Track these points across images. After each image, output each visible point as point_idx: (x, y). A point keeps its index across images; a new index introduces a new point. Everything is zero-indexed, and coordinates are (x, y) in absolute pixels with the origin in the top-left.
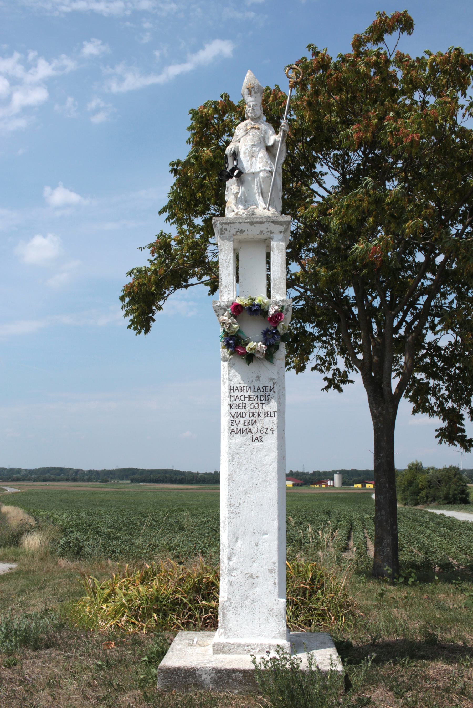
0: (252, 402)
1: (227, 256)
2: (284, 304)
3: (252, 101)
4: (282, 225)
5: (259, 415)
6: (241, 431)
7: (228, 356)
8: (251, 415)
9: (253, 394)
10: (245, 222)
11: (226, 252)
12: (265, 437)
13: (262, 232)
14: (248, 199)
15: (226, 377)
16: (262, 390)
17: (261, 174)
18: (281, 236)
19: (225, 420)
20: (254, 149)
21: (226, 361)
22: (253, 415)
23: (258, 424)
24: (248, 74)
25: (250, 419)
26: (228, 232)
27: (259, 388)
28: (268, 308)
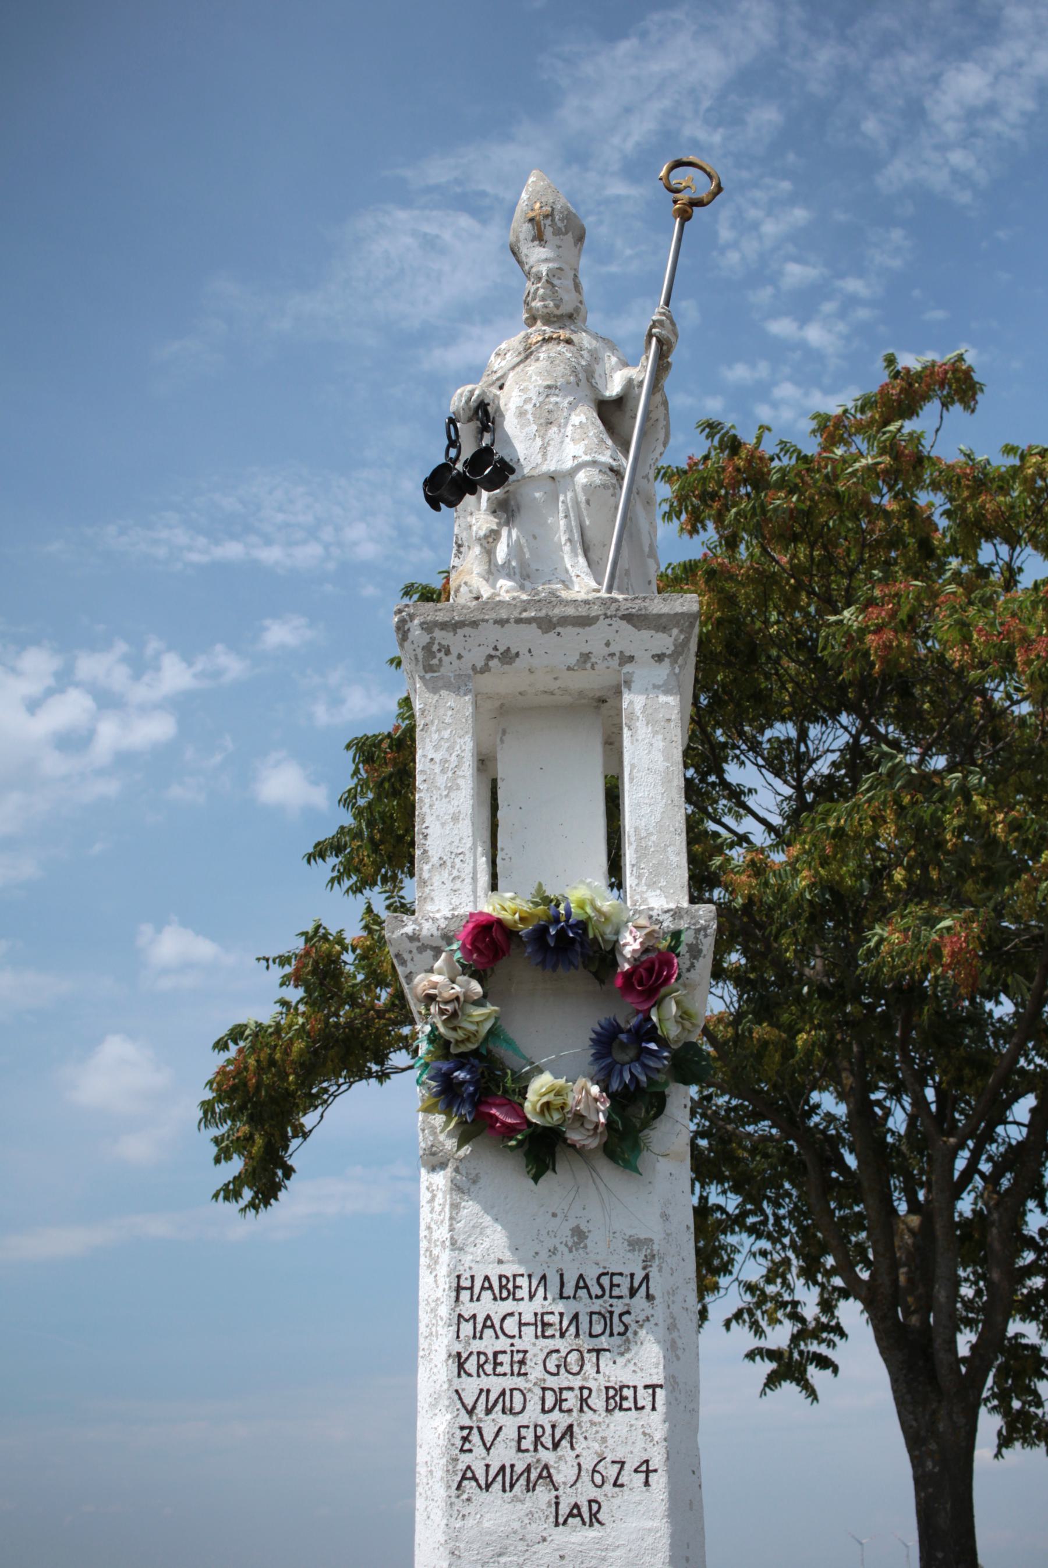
0: (551, 1344)
1: (450, 749)
2: (683, 925)
3: (546, 260)
4: (664, 629)
5: (583, 1401)
6: (505, 1477)
7: (450, 1144)
8: (550, 1402)
9: (560, 1307)
10: (519, 621)
11: (446, 734)
12: (612, 1504)
13: (585, 657)
14: (534, 566)
15: (442, 1233)
16: (596, 1290)
17: (582, 478)
18: (663, 671)
19: (434, 1428)
20: (553, 399)
21: (443, 1166)
22: (559, 1401)
23: (580, 1445)
24: (532, 179)
25: (545, 1420)
26: (453, 657)
27: (581, 1283)
28: (617, 933)
